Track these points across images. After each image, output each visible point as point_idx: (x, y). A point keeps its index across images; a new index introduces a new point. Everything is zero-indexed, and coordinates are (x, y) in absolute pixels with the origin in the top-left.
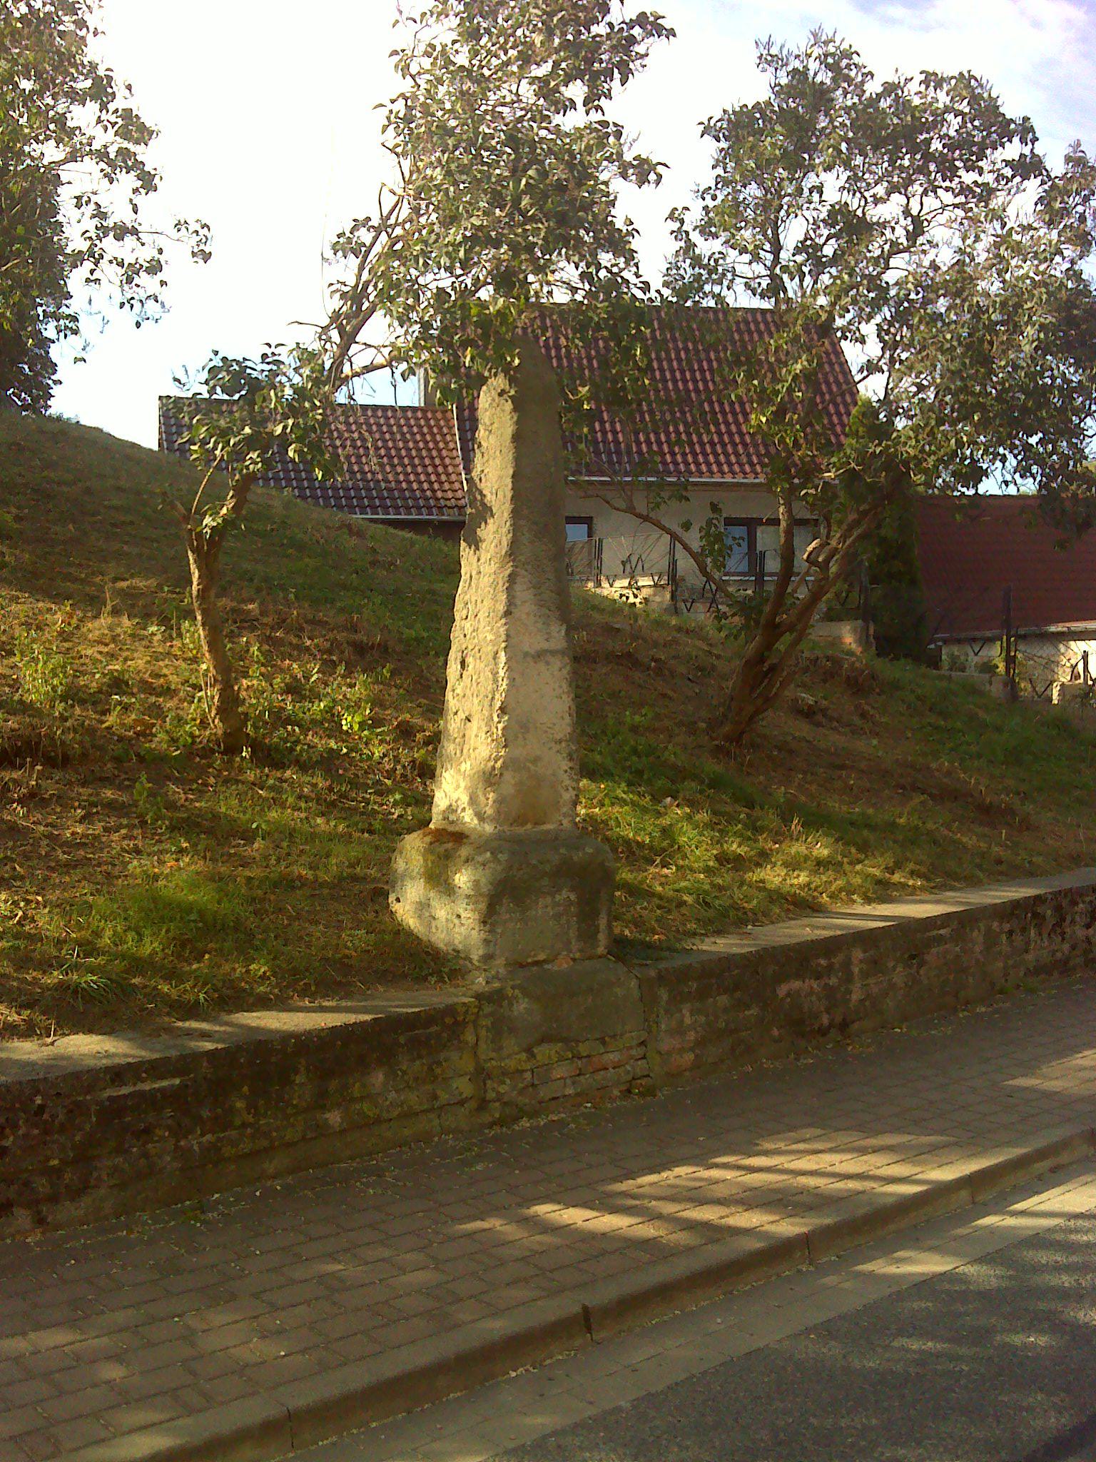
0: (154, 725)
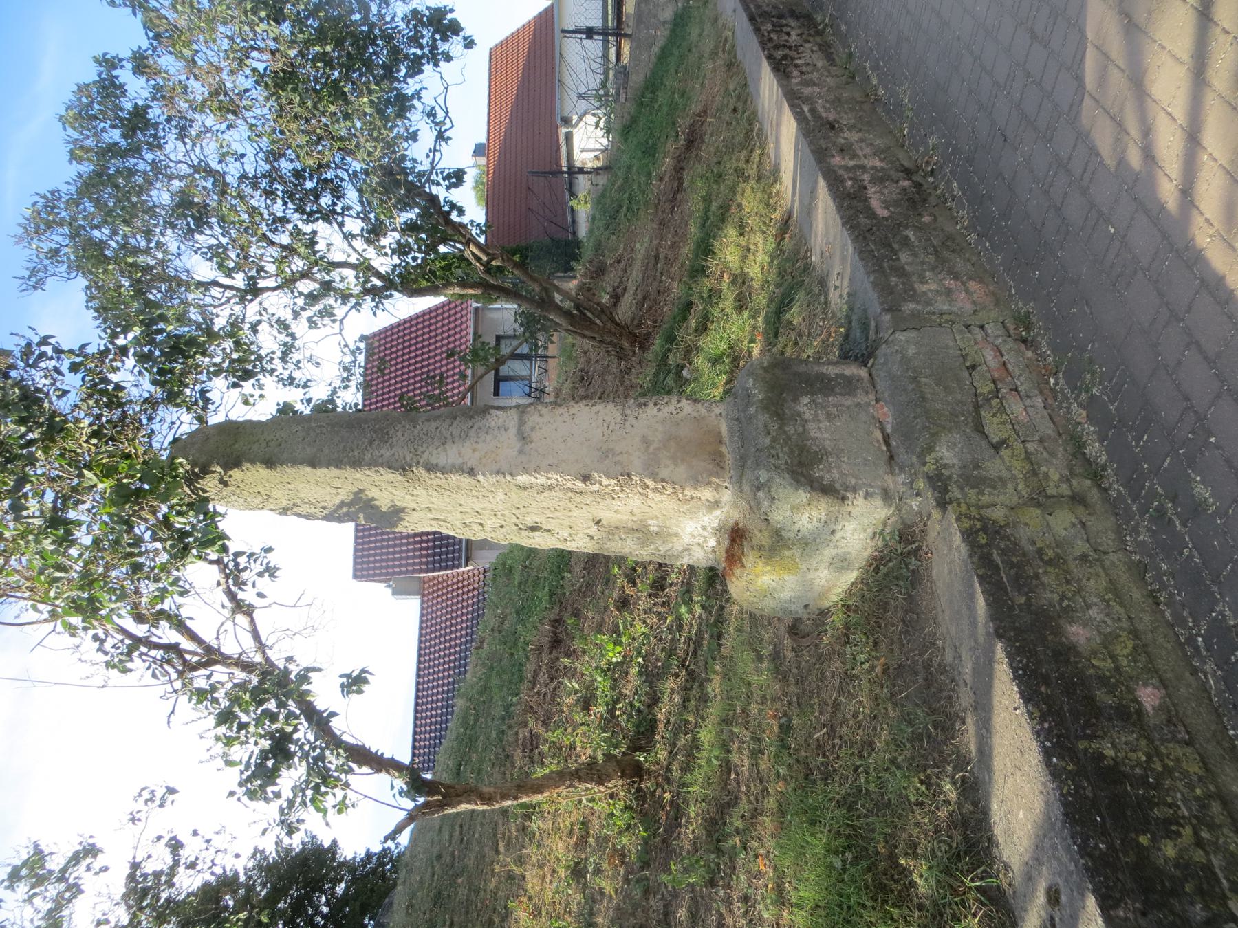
0: (613, 845)
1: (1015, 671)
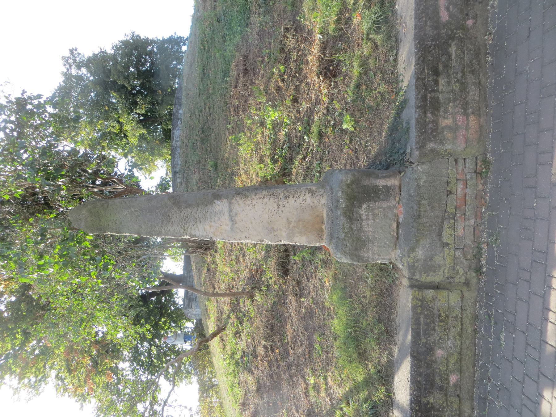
1: (412, 371)
